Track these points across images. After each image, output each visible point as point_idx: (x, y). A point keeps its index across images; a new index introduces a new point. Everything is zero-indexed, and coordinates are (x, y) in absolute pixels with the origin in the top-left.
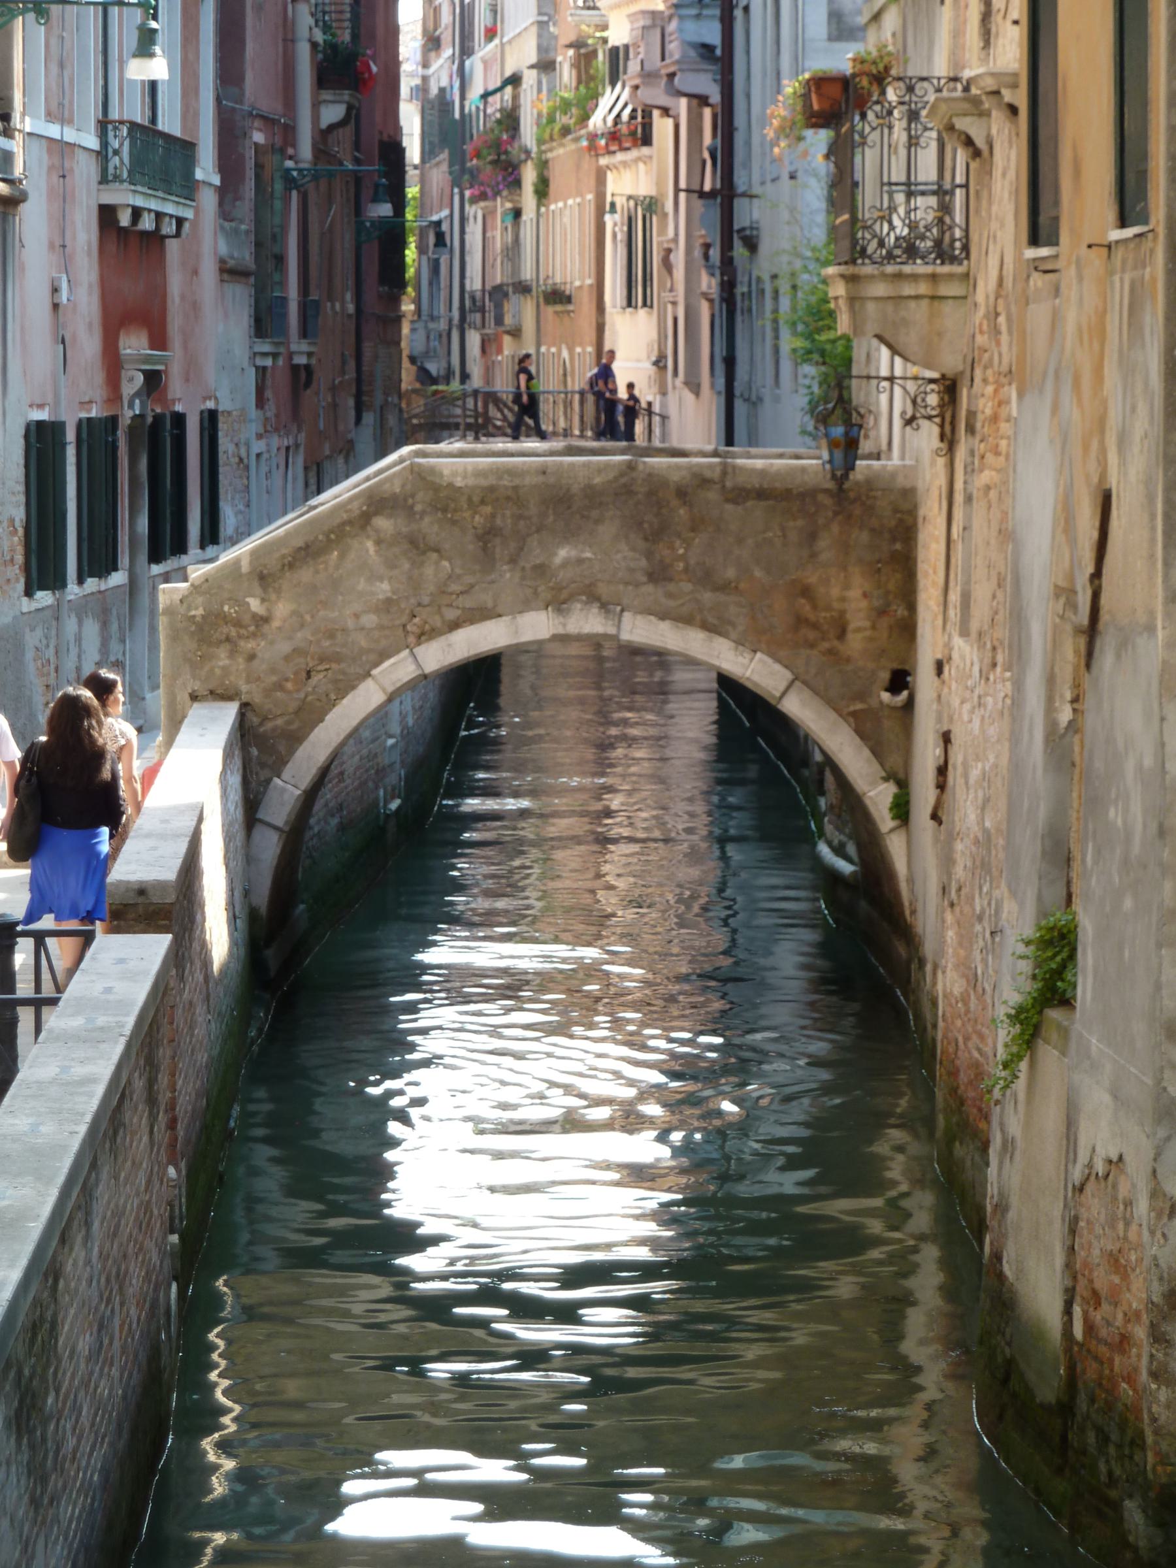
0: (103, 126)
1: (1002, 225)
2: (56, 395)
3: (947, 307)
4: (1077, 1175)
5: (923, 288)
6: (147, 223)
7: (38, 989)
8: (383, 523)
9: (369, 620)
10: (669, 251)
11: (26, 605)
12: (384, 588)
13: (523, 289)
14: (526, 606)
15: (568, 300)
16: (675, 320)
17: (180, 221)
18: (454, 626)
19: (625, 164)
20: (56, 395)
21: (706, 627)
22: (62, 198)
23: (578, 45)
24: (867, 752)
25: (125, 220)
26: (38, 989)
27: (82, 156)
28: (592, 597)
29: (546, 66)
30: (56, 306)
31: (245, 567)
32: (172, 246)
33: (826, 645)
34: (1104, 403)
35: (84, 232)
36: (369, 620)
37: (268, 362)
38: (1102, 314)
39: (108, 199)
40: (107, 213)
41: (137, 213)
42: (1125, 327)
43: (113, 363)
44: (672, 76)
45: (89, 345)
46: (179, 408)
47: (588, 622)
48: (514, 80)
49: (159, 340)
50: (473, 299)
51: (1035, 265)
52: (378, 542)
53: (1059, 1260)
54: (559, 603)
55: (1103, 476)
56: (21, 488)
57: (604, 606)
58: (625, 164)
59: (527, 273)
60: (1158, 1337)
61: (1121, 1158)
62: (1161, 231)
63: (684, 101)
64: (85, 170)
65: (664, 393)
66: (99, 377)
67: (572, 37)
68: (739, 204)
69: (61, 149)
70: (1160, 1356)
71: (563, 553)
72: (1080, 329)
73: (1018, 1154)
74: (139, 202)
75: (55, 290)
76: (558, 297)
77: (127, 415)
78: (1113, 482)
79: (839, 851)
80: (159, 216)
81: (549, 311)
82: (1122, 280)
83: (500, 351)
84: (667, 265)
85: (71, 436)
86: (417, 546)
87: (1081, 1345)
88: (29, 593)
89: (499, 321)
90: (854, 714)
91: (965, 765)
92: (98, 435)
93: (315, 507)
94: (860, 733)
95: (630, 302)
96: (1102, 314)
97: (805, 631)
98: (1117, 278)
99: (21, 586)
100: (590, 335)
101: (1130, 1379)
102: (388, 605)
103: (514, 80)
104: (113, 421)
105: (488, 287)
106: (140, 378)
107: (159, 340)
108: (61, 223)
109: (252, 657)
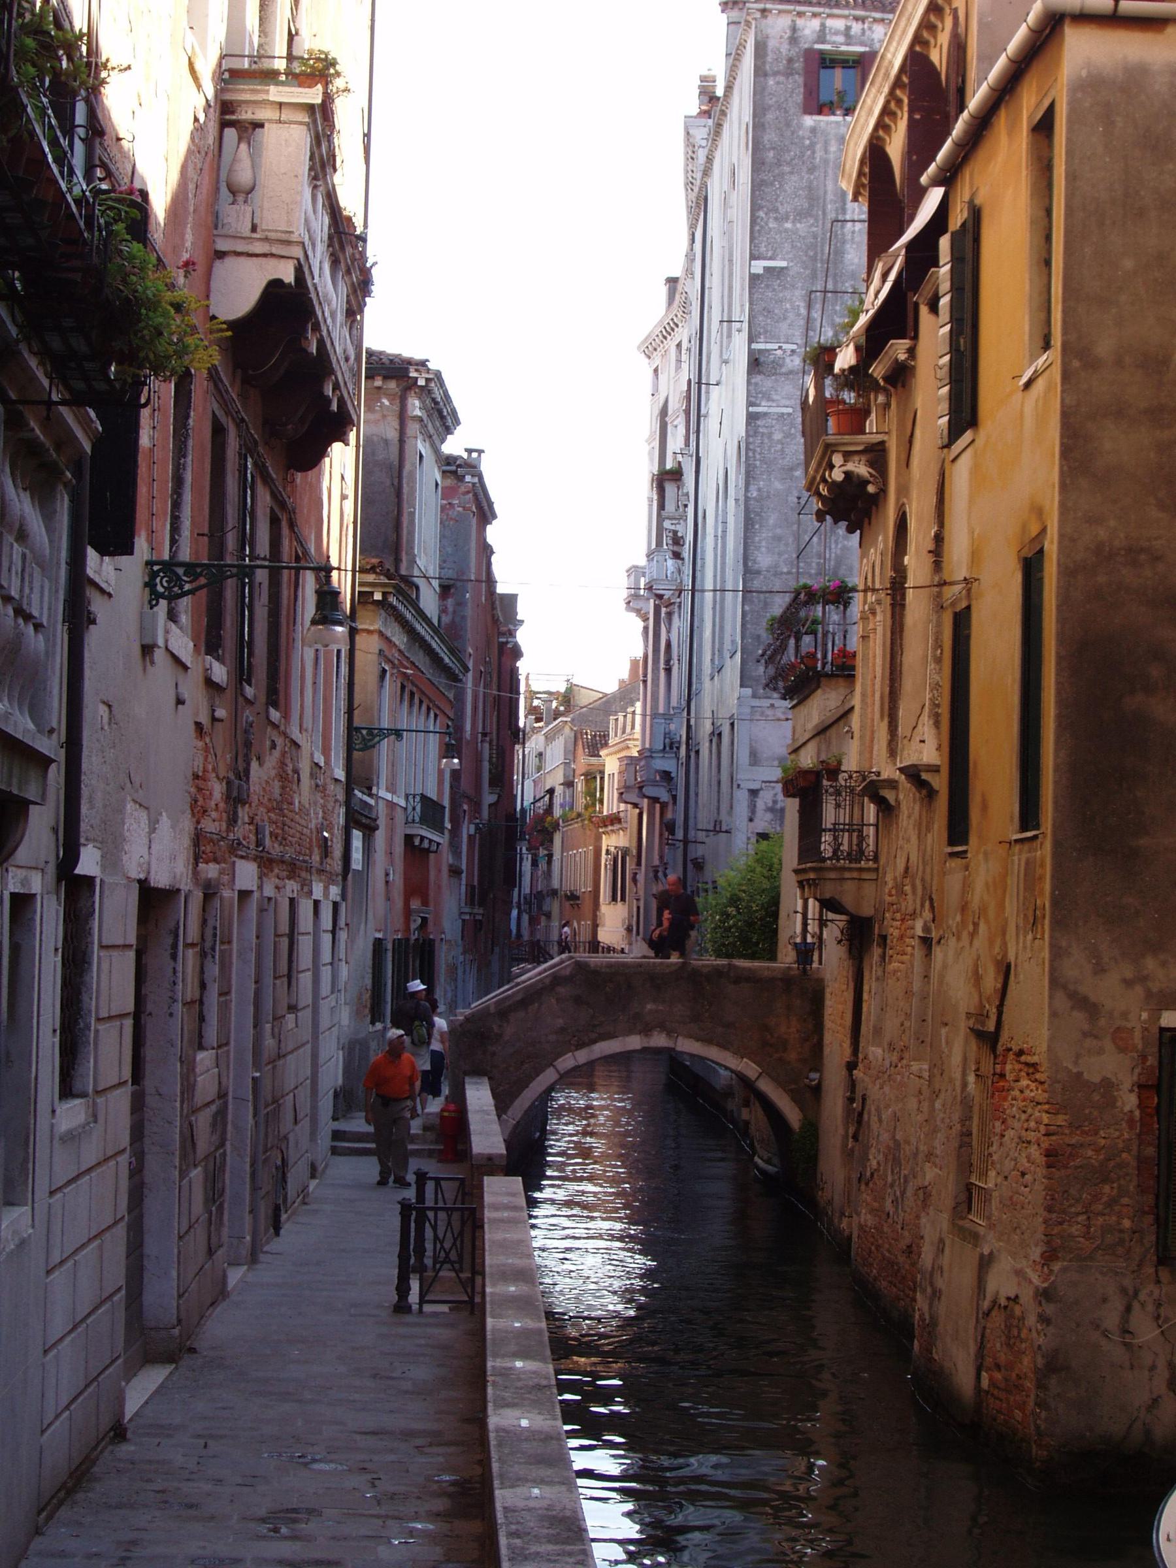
0: (407, 796)
1: (908, 841)
2: (386, 926)
3: (866, 885)
4: (986, 1305)
5: (855, 875)
6: (426, 844)
7: (436, 1203)
8: (562, 990)
9: (552, 1038)
10: (636, 874)
11: (371, 1029)
12: (560, 1022)
13: (554, 893)
14: (630, 1032)
15: (578, 898)
16: (638, 908)
17: (438, 844)
18: (594, 1042)
19: (612, 831)
20: (386, 926)
21: (719, 1045)
22: (391, 830)
23: (586, 775)
24: (797, 1109)
25: (417, 842)
26: (436, 1203)
27: (399, 809)
28: (662, 1027)
29: (569, 784)
30: (387, 882)
31: (492, 1010)
32: (432, 856)
33: (776, 1056)
34: (1006, 921)
35: (399, 848)
36: (552, 1038)
37: (467, 917)
38: (1004, 876)
39: (409, 832)
40: (409, 838)
41: (422, 838)
42: (1022, 881)
43: (408, 913)
44: (641, 788)
45: (399, 903)
46: (431, 937)
47: (659, 1040)
48: (551, 792)
49: (425, 903)
50: (525, 898)
51: (952, 855)
52: (557, 1000)
53: (973, 1348)
54: (646, 1031)
55: (1005, 955)
56: (370, 971)
57: (669, 1034)
58: (612, 831)
59: (556, 884)
60: (1041, 1386)
61: (1017, 1297)
62: (1049, 832)
63: (646, 800)
64: (400, 816)
65: (630, 944)
66: (402, 920)
67: (583, 771)
68: (691, 847)
69: (391, 805)
70: (1042, 1395)
71: (649, 1007)
72: (987, 884)
73: (943, 1298)
74: (424, 833)
75: (387, 875)
76: (573, 897)
77: (413, 938)
78: (1011, 957)
79: (768, 1162)
80: (431, 841)
81: (567, 904)
82: (1019, 860)
83: (539, 924)
84: (634, 880)
85: (390, 946)
86: (578, 1001)
87: (987, 1392)
88: (373, 1023)
89: (540, 908)
90: (791, 1090)
91: (878, 1110)
92: (401, 946)
93: (518, 984)
94: (794, 1100)
95: (614, 899)
96: (1004, 876)
97: (766, 1048)
98: (1016, 858)
99: (369, 1019)
100: (590, 915)
101: (1022, 1407)
102: (562, 1030)
103: (551, 792)
104: (408, 940)
105: (534, 892)
106: (420, 920)
107: (425, 903)
108: (390, 841)
109: (494, 1054)
